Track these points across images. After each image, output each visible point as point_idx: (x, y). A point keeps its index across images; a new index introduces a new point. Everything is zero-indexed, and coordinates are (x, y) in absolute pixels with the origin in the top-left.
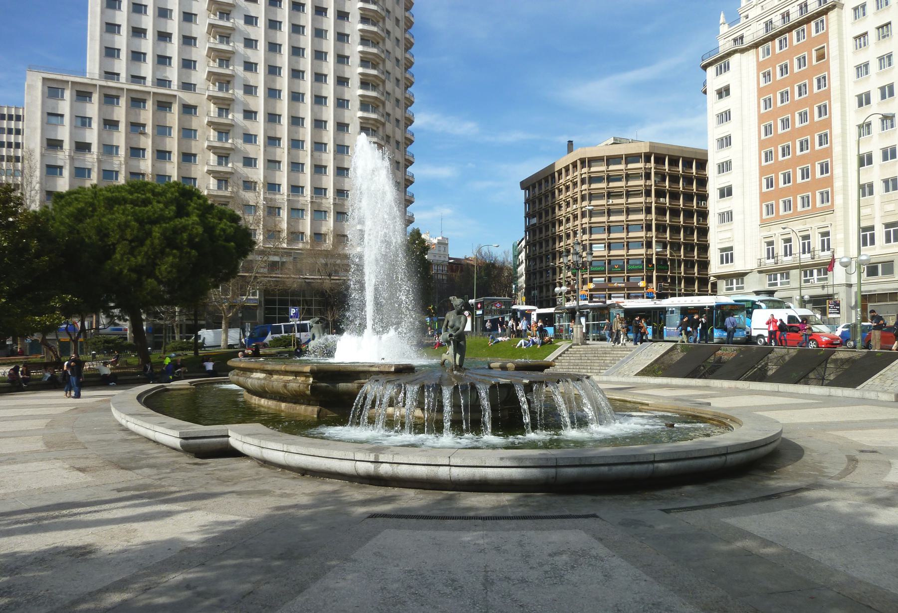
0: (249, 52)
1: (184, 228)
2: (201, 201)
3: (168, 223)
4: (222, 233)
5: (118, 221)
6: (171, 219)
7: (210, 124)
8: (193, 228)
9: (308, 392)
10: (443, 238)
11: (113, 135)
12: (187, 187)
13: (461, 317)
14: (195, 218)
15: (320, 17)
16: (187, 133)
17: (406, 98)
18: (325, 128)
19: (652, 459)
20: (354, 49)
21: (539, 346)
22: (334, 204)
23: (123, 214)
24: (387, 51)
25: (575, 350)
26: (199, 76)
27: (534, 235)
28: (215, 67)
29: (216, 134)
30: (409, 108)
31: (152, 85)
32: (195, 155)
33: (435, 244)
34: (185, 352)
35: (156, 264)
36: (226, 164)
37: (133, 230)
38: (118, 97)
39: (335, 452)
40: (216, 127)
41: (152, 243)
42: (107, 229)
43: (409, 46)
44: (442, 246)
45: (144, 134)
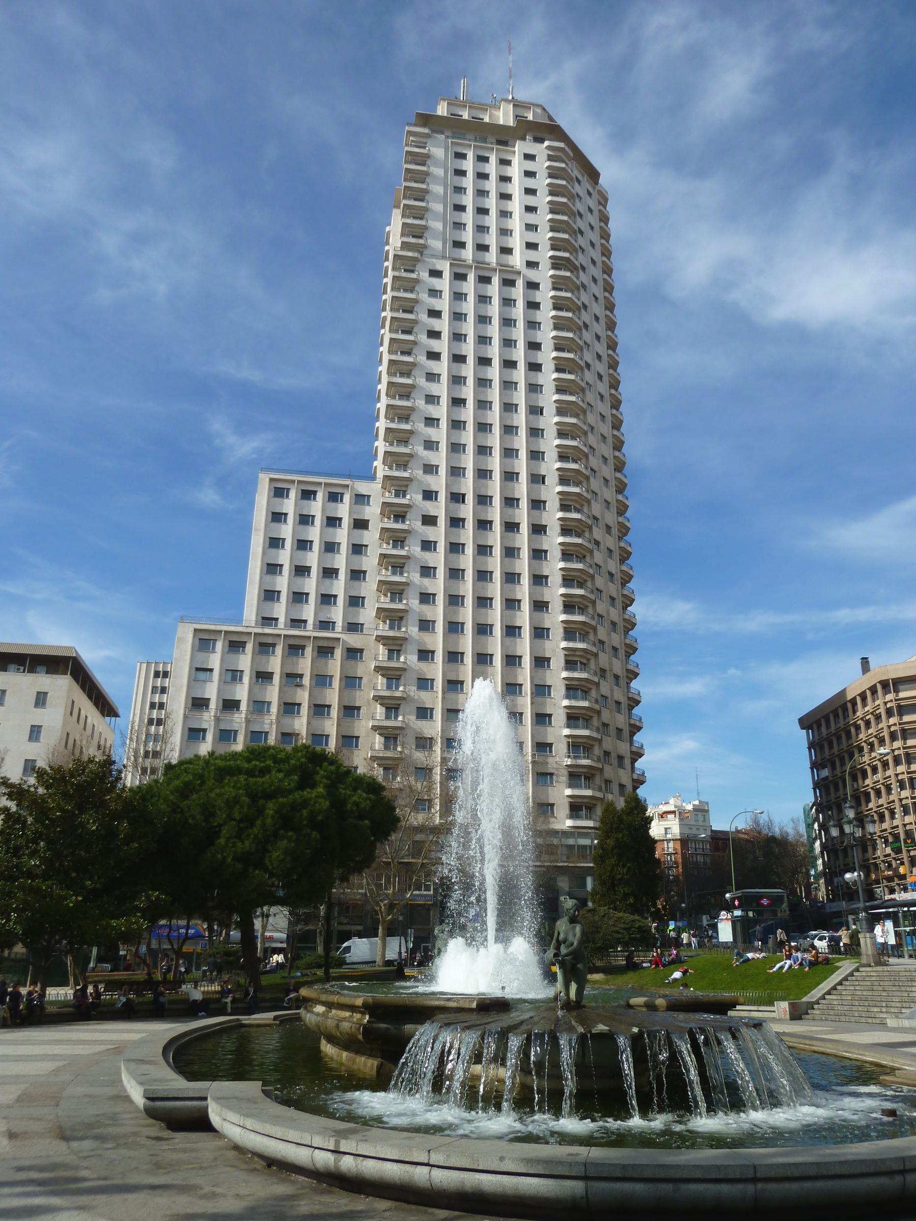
0: (426, 581)
1: (305, 803)
2: (333, 768)
3: (286, 797)
4: (355, 808)
5: (227, 796)
6: (290, 792)
7: (378, 669)
8: (315, 802)
9: (360, 1037)
10: (700, 802)
11: (266, 689)
12: (318, 748)
13: (575, 927)
14: (320, 789)
15: (511, 534)
16: (351, 682)
17: (624, 620)
18: (520, 665)
19: (750, 1175)
20: (555, 566)
21: (807, 969)
22: (533, 762)
23: (234, 787)
24: (596, 565)
25: (864, 974)
26: (367, 615)
27: (828, 793)
28: (386, 602)
29: (385, 680)
30: (630, 633)
31: (314, 628)
32: (359, 708)
33: (689, 811)
34: (313, 971)
35: (268, 851)
36: (396, 717)
37: (242, 807)
38: (274, 645)
39: (291, 1131)
40: (384, 672)
41: (264, 824)
42: (214, 806)
43: (625, 556)
44: (700, 814)
45: (300, 686)
